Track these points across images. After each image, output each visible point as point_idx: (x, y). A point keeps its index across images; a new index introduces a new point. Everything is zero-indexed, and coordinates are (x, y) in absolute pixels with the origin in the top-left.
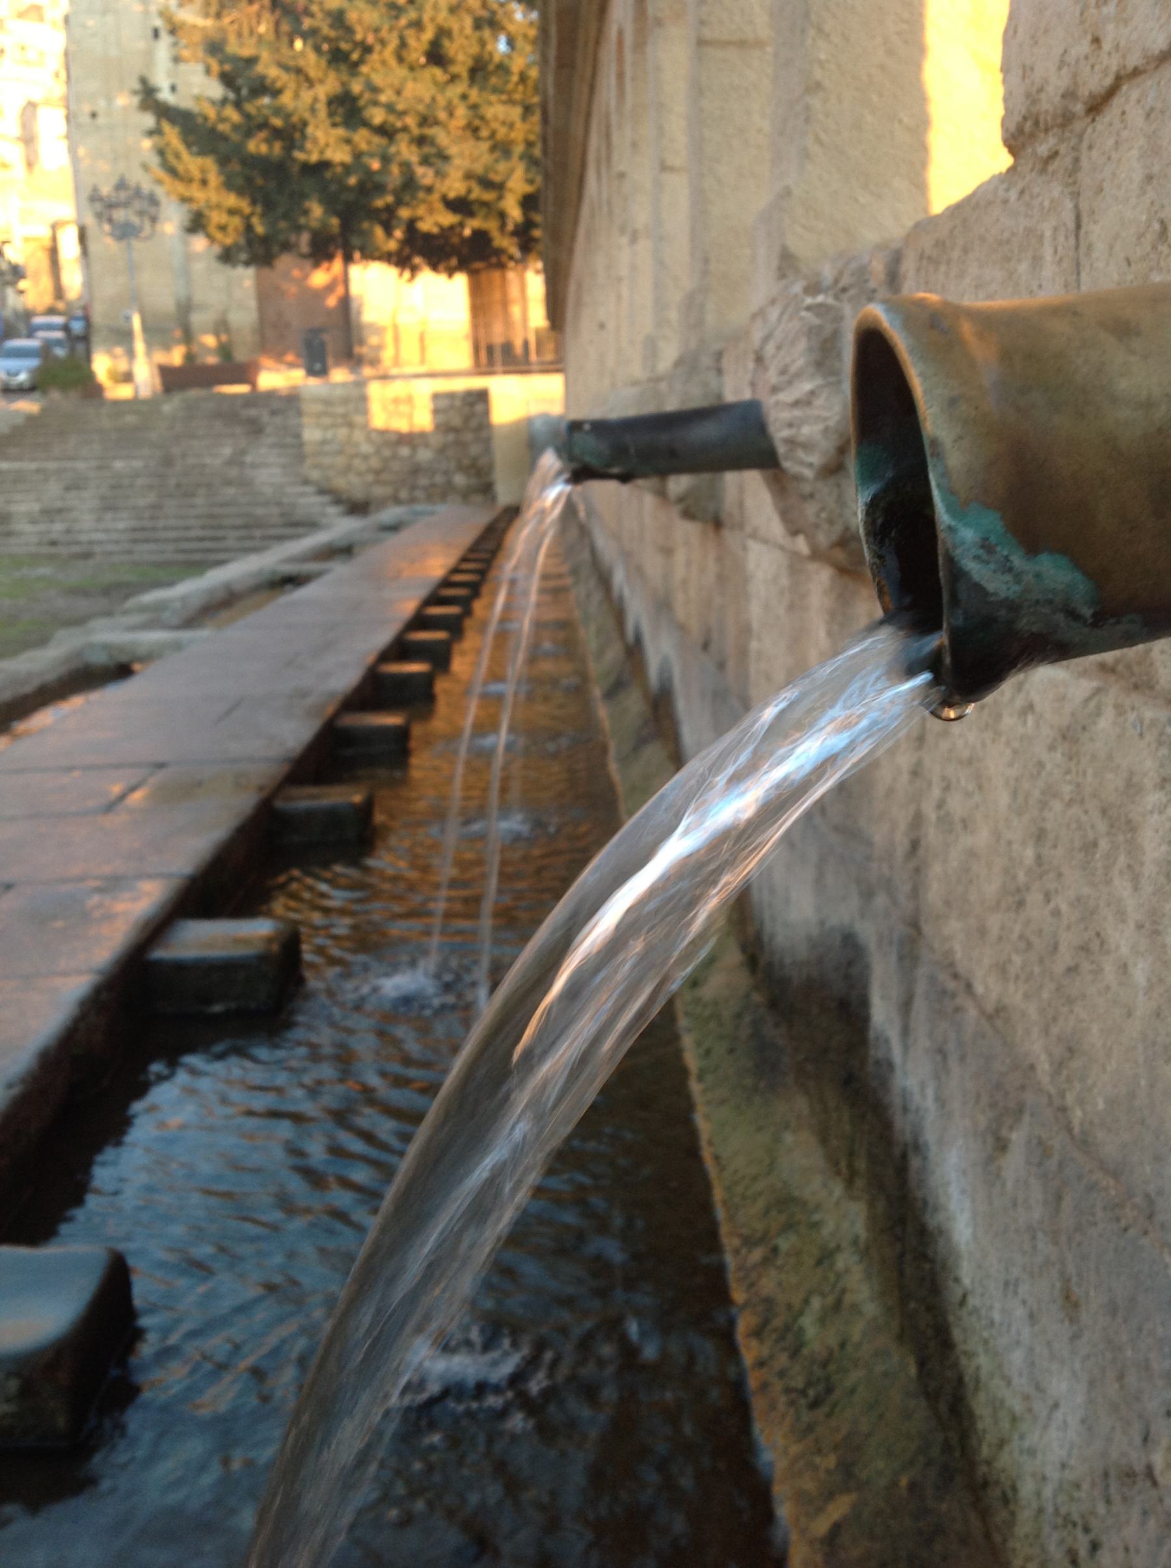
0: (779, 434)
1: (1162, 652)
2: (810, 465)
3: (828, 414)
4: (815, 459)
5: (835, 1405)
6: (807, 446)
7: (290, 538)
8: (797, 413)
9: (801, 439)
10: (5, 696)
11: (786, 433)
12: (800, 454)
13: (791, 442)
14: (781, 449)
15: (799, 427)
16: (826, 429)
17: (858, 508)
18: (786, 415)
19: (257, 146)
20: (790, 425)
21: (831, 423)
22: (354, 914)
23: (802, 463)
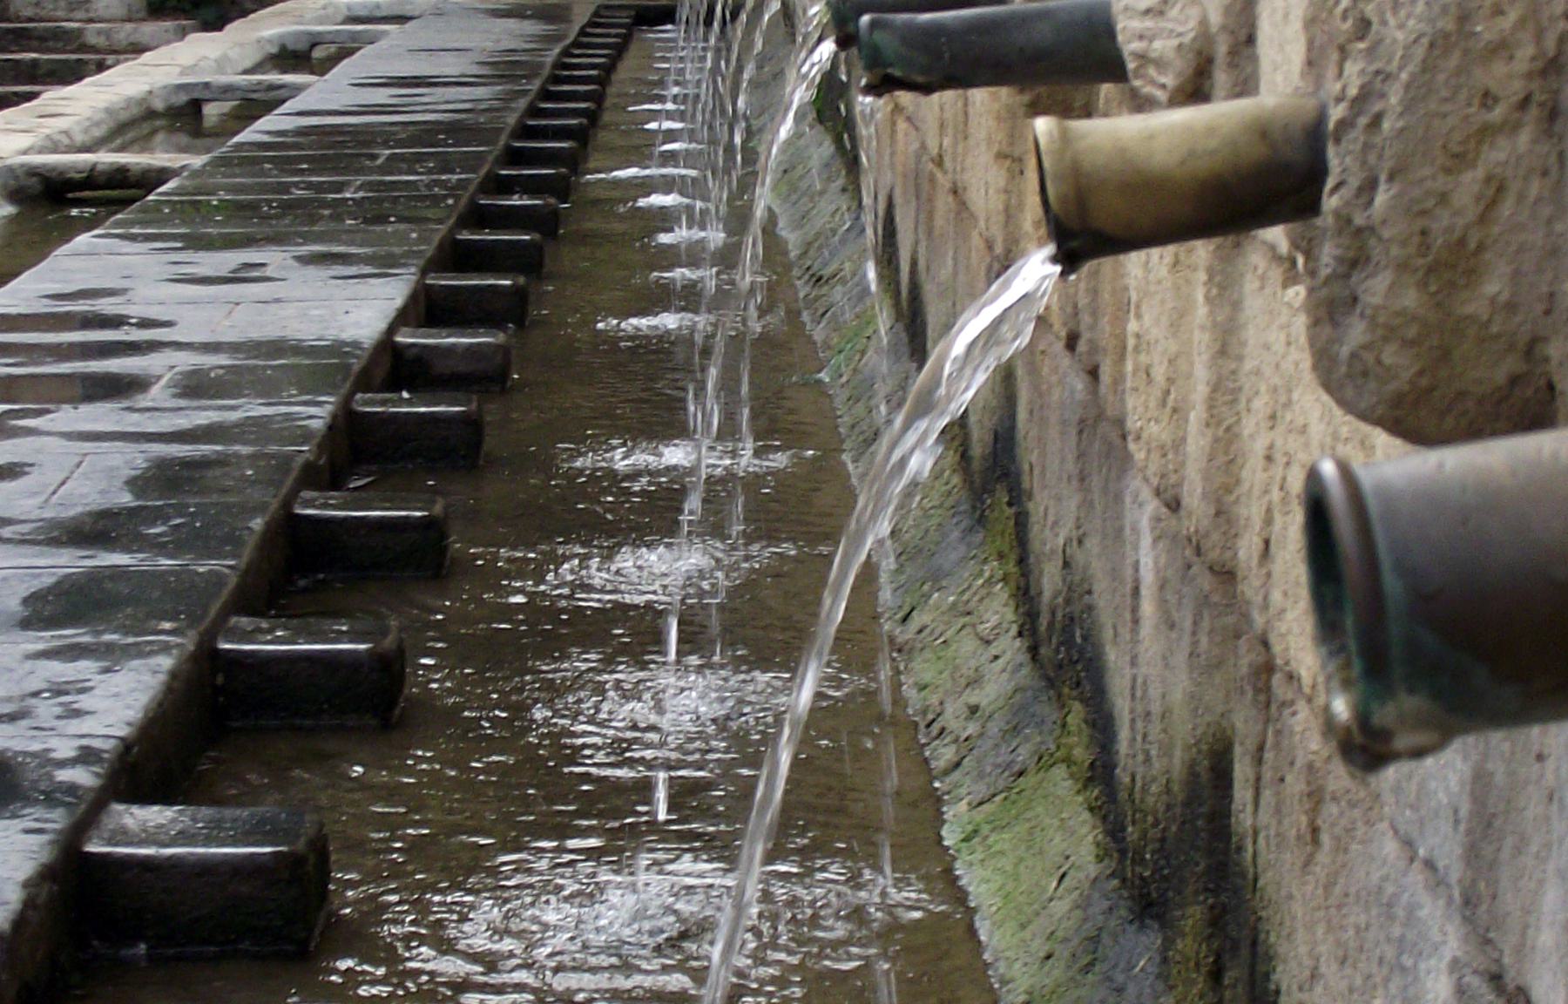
0: (1129, 47)
1: (1297, 294)
2: (1163, 86)
3: (1180, 29)
4: (1169, 80)
5: (1457, 822)
6: (1160, 64)
7: (151, 114)
8: (1149, 23)
9: (1153, 55)
10: (7, 514)
11: (1136, 46)
12: (1152, 71)
13: (1142, 57)
14: (1131, 65)
15: (1151, 41)
16: (1180, 46)
17: (880, 542)
18: (1137, 24)
19: (1358, 791)
20: (1141, 37)
21: (1187, 39)
22: (1222, 288)
23: (1153, 82)
